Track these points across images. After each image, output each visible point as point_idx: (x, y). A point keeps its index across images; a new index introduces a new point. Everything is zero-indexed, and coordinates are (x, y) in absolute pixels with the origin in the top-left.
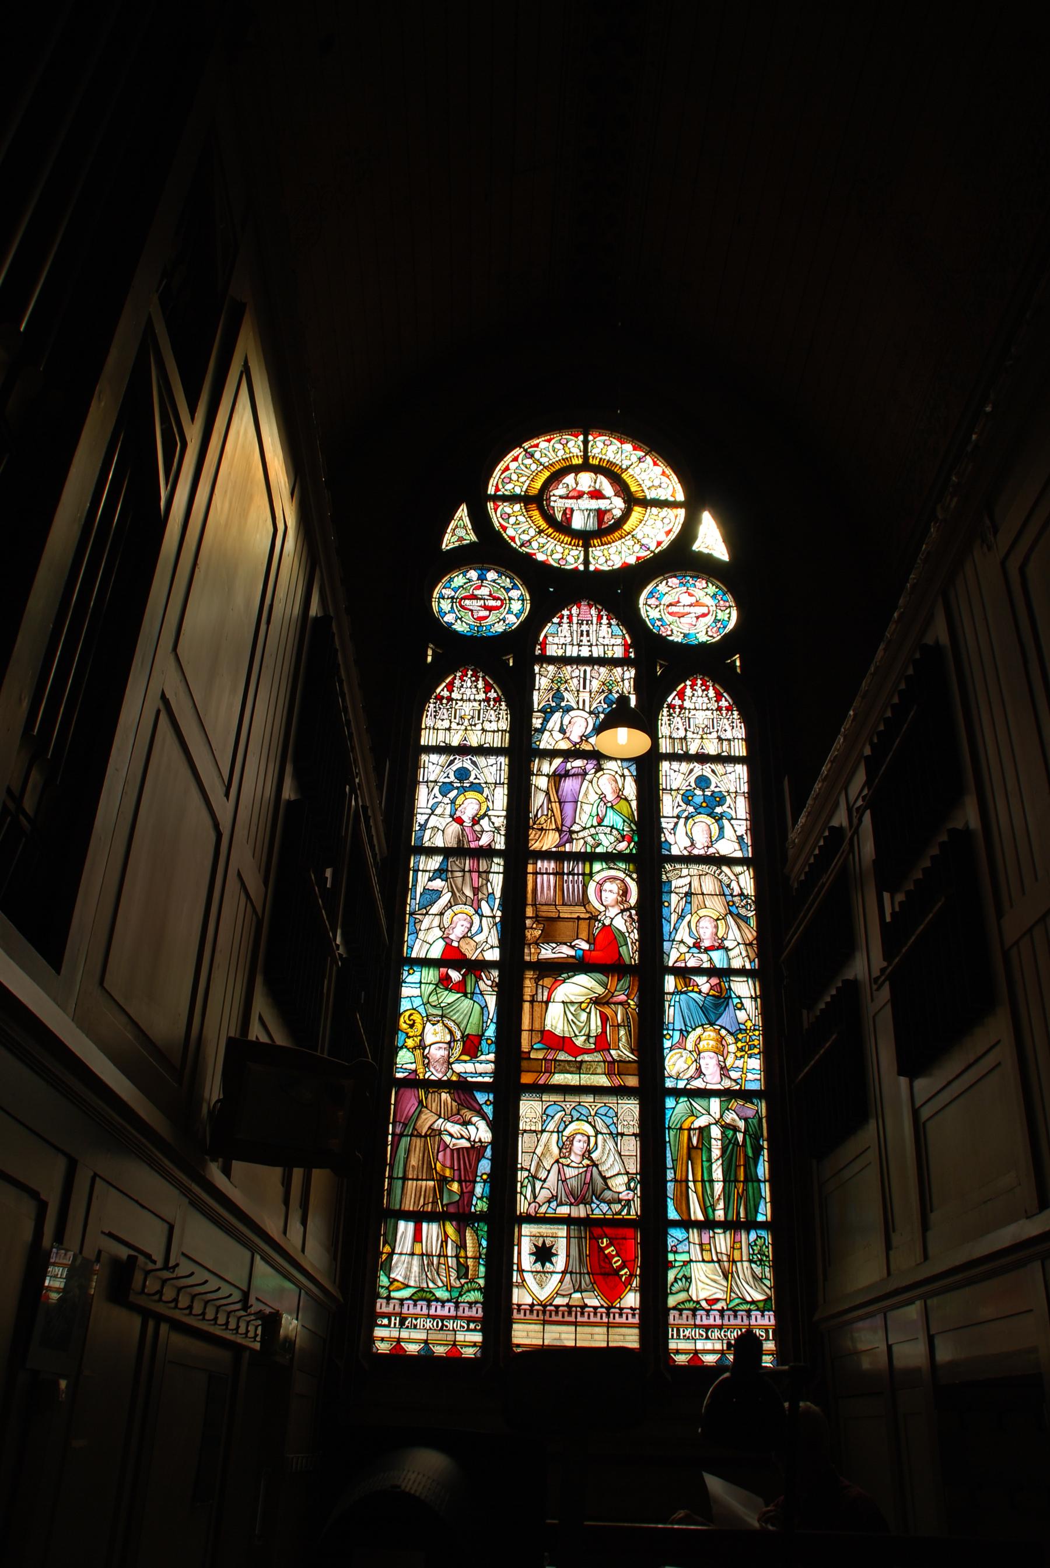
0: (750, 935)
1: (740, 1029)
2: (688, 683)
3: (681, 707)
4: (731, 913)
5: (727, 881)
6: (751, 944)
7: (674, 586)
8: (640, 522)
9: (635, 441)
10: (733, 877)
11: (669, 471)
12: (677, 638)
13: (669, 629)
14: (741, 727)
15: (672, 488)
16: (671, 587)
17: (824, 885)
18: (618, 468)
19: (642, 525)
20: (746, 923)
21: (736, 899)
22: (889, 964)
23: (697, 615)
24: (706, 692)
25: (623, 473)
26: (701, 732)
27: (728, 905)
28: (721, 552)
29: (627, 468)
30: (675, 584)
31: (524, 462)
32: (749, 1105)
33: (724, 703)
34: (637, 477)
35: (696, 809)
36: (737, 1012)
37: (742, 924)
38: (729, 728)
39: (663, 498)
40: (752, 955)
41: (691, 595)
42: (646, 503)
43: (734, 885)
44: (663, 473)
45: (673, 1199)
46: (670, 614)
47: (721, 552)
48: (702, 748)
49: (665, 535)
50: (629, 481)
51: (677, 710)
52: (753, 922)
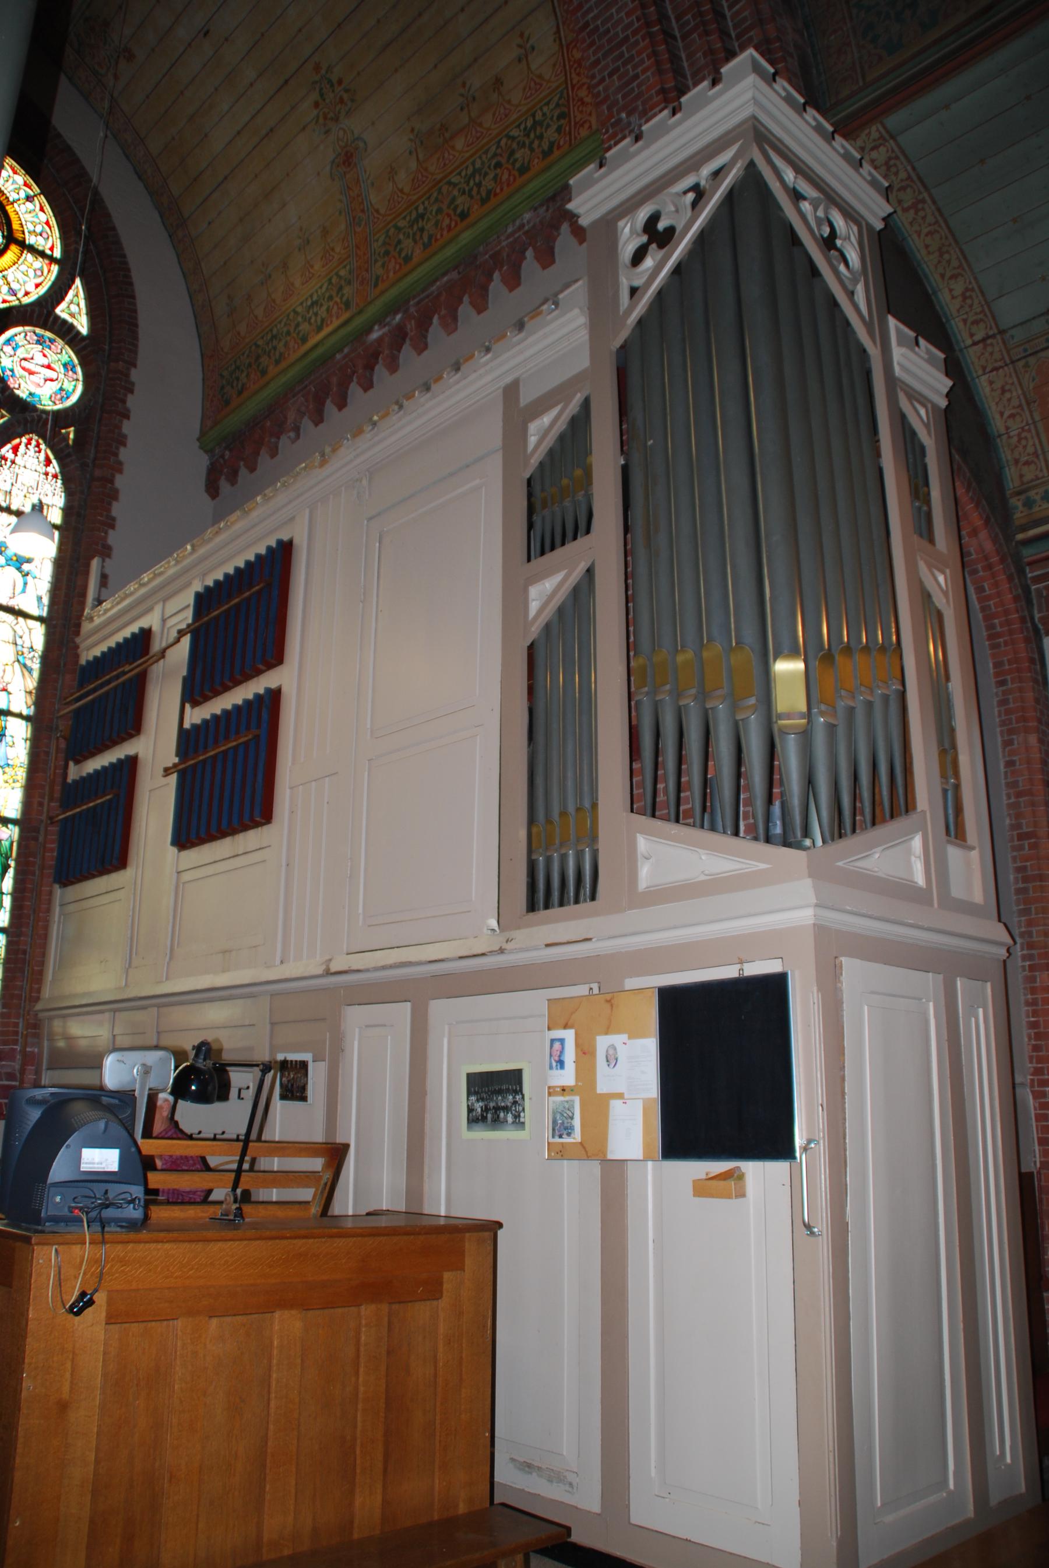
0: (32, 683)
1: (9, 765)
2: (24, 440)
3: (13, 462)
4: (18, 661)
5: (21, 633)
6: (30, 693)
7: (31, 342)
8: (14, 264)
9: (27, 176)
10: (27, 631)
11: (53, 222)
12: (22, 394)
13: (18, 382)
14: (61, 497)
15: (52, 242)
16: (29, 342)
17: (124, 673)
18: (4, 197)
19: (15, 267)
20: (30, 673)
21: (26, 650)
22: (181, 762)
23: (46, 377)
24: (37, 454)
25: (8, 205)
26: (25, 491)
27: (18, 654)
28: (82, 325)
29: (14, 202)
30: (33, 340)
31: (19, 287)
32: (4, 829)
33: (50, 470)
34: (21, 216)
35: (7, 560)
36: (8, 748)
37: (26, 673)
38: (50, 494)
39: (41, 248)
40: (30, 702)
41: (45, 355)
42: (23, 245)
43: (26, 638)
44: (47, 223)
45: (328, 973)
46: (24, 369)
47: (82, 325)
48: (23, 506)
49: (34, 287)
50: (12, 216)
51: (9, 463)
52: (36, 674)
